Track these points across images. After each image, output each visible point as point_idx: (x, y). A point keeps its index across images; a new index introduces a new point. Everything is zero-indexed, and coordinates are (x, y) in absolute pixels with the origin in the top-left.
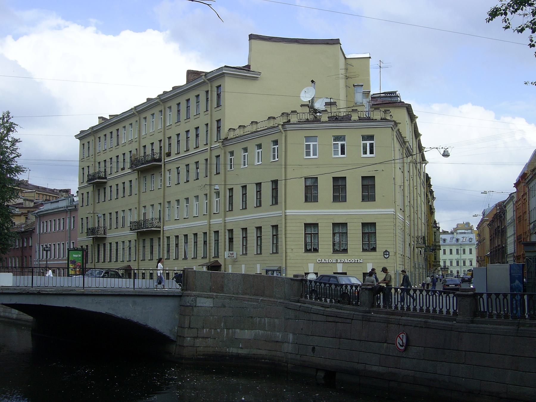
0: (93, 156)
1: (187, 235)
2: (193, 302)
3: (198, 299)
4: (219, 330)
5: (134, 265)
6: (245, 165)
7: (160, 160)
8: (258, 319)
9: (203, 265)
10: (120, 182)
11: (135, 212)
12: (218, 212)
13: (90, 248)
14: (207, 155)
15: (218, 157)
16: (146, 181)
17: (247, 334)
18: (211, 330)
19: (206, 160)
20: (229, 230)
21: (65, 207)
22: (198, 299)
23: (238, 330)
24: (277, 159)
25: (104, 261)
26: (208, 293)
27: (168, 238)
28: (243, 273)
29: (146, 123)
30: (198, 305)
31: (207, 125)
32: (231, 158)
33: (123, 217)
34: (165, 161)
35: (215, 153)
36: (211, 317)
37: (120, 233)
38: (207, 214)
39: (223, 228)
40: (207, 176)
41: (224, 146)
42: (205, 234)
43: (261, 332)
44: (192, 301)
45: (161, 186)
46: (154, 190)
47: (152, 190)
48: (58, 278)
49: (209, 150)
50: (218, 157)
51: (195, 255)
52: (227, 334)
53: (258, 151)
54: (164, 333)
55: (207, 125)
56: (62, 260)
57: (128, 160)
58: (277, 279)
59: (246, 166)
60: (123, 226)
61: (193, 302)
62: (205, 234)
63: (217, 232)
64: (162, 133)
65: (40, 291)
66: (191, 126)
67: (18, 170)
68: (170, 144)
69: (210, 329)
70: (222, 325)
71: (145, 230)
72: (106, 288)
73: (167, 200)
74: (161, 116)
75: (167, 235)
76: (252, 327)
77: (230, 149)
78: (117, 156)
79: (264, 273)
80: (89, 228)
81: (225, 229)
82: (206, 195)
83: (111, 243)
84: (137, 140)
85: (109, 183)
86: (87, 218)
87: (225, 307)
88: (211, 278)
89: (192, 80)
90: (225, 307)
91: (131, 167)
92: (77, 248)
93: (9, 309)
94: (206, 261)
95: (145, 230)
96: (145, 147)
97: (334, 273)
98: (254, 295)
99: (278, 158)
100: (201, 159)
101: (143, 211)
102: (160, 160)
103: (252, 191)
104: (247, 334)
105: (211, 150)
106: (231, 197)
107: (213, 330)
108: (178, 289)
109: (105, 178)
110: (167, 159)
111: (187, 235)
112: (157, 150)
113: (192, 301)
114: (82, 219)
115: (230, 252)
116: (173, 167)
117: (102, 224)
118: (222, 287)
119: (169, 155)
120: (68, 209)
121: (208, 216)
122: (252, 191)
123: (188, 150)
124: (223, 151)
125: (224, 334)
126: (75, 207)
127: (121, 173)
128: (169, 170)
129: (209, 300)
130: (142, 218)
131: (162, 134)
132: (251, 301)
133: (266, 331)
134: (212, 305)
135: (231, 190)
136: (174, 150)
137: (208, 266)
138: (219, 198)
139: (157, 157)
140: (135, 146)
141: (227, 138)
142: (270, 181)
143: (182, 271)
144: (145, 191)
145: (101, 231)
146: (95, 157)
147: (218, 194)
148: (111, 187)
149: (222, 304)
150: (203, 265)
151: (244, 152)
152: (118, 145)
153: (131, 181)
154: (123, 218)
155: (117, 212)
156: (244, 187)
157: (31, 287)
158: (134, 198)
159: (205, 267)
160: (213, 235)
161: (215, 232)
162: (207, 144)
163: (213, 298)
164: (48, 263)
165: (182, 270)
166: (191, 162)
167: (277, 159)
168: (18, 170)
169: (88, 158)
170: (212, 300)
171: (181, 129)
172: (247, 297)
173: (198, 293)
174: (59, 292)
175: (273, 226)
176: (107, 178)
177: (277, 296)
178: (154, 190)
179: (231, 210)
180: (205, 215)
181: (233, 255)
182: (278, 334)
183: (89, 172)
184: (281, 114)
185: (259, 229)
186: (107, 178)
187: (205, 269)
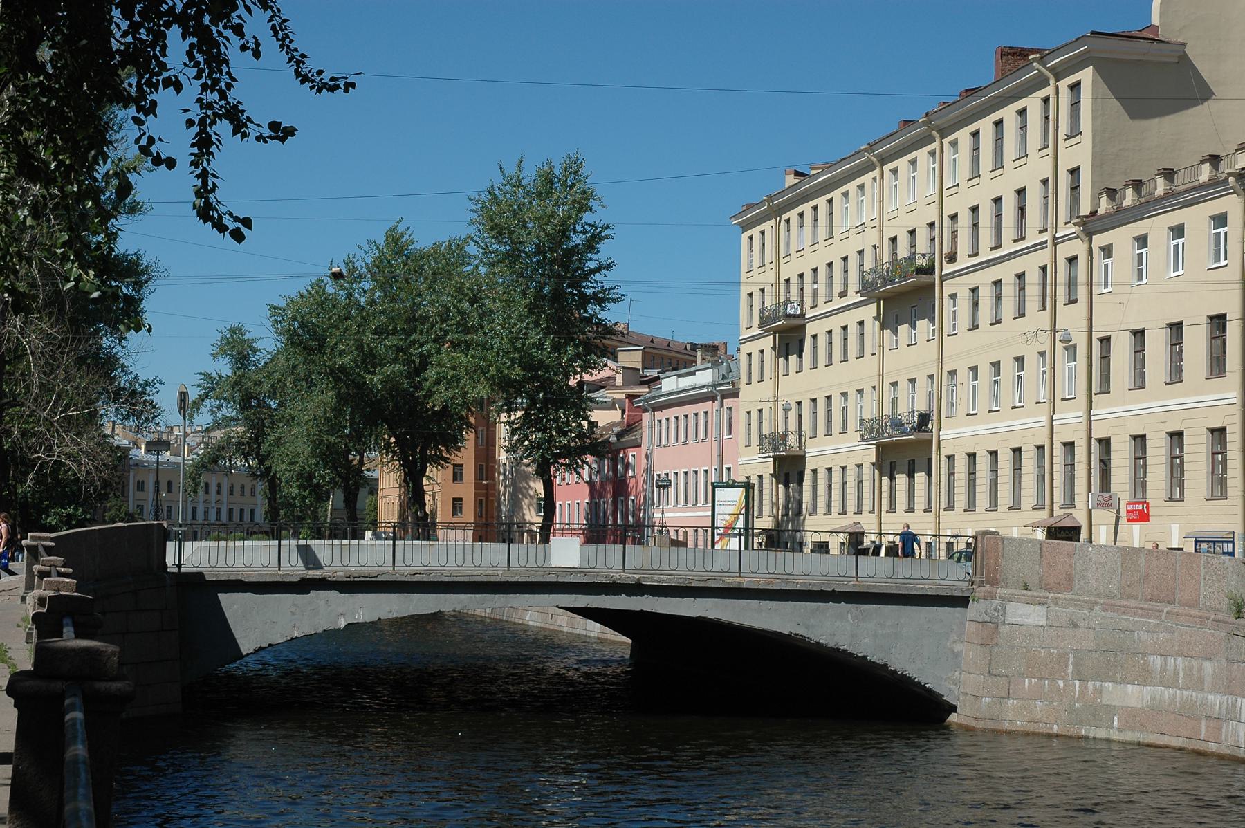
0: (773, 265)
1: (1143, 437)
2: (996, 614)
3: (1011, 607)
4: (1061, 683)
5: (868, 523)
6: (1176, 269)
7: (929, 270)
8: (1159, 660)
9: (1034, 526)
10: (835, 323)
11: (870, 398)
12: (1073, 396)
13: (766, 480)
14: (1044, 257)
15: (1072, 260)
16: (954, 306)
17: (1134, 695)
18: (1042, 683)
19: (1044, 269)
20: (1100, 441)
21: (708, 386)
22: (1011, 607)
23: (1109, 685)
24: (1223, 263)
25: (829, 513)
26: (1035, 594)
27: (950, 458)
28: (1136, 545)
29: (897, 182)
30: (1010, 619)
31: (1045, 182)
32: (1140, 251)
33: (843, 408)
34: (1057, 235)
35: (1065, 251)
36: (1043, 651)
37: (958, 431)
38: (1021, 404)
39: (1084, 435)
40: (1045, 308)
41: (1089, 235)
42: (1040, 448)
43: (1168, 693)
44: (996, 610)
45: (933, 335)
46: (916, 344)
47: (913, 343)
48: (532, 547)
49: (1049, 244)
50: (1072, 260)
51: (1016, 501)
52: (1082, 693)
53: (1140, 251)
54: (927, 686)
55: (1045, 182)
56: (700, 509)
57: (853, 277)
58: (1208, 563)
59: (1110, 289)
60: (844, 430)
61: (996, 614)
62: (1040, 448)
63: (1069, 446)
64: (935, 206)
65: (642, 580)
66: (1005, 186)
67: (601, 299)
68: (954, 233)
69: (1041, 679)
70: (1070, 670)
71: (894, 439)
72: (710, 573)
73: (947, 368)
74: (934, 163)
75: (945, 451)
76: (1145, 677)
77: (1099, 240)
78: (912, 233)
79: (1189, 546)
80: (765, 435)
81: (1090, 437)
82: (1042, 354)
83: (814, 471)
84: (876, 223)
85: (811, 329)
86: (760, 411)
87: (1075, 626)
88: (1041, 557)
89: (1009, 73)
90: (1075, 626)
91: (762, 324)
92: (734, 481)
93: (580, 621)
94: (1043, 515)
95: (894, 439)
96: (954, 217)
97: (1169, 549)
98: (1150, 600)
99: (1226, 259)
100: (1030, 265)
101: (888, 393)
102: (929, 270)
103: (1157, 345)
104: (1134, 695)
105: (1055, 245)
106: (1105, 358)
107: (1047, 682)
108: (962, 581)
109: (802, 316)
110: (948, 269)
111: (1143, 437)
112: (922, 246)
113: (996, 610)
114: (749, 413)
115: (1101, 494)
116: (960, 286)
117: (793, 426)
118: (1070, 579)
119: (952, 258)
120: (718, 391)
121: (1047, 406)
122: (1157, 345)
123: (998, 246)
124: (1085, 246)
125: (1075, 694)
126: (733, 386)
127: (838, 303)
128: (954, 296)
129: (1038, 608)
130: (887, 411)
131: (935, 207)
132: (1141, 616)
133: (1179, 689)
134: (1043, 622)
135: (1105, 341)
136: (964, 247)
137: (1049, 528)
138: (1075, 361)
139: (922, 262)
140: (872, 237)
141: (1097, 212)
142: (1165, 326)
143: (898, 537)
144: (897, 345)
145: (792, 441)
146: (778, 266)
147: (1072, 350)
148: (815, 337)
149: (1071, 619)
150: (1034, 526)
151: (1216, 226)
152: (831, 236)
153: (861, 323)
154: (844, 410)
155: (829, 398)
156: (1139, 334)
157: (738, 575)
158: (870, 363)
159: (1041, 529)
160: (1059, 451)
161: (1065, 444)
162: (1045, 230)
163: (1046, 606)
164: (666, 515)
165: (897, 534)
166: (1005, 273)
167: (1145, 281)
168: (601, 299)
169: (762, 269)
170: (1044, 608)
171: (982, 195)
172: (1132, 603)
173: (1010, 591)
174: (683, 583)
175: (1212, 431)
176: (807, 317)
177: (1208, 604)
178: (916, 344)
179: (1105, 388)
180: (1040, 403)
181: (1110, 502)
182: (1210, 697)
183: (763, 302)
184: (1236, 148)
185: (1139, 440)
186: (807, 317)
187: (1040, 535)
